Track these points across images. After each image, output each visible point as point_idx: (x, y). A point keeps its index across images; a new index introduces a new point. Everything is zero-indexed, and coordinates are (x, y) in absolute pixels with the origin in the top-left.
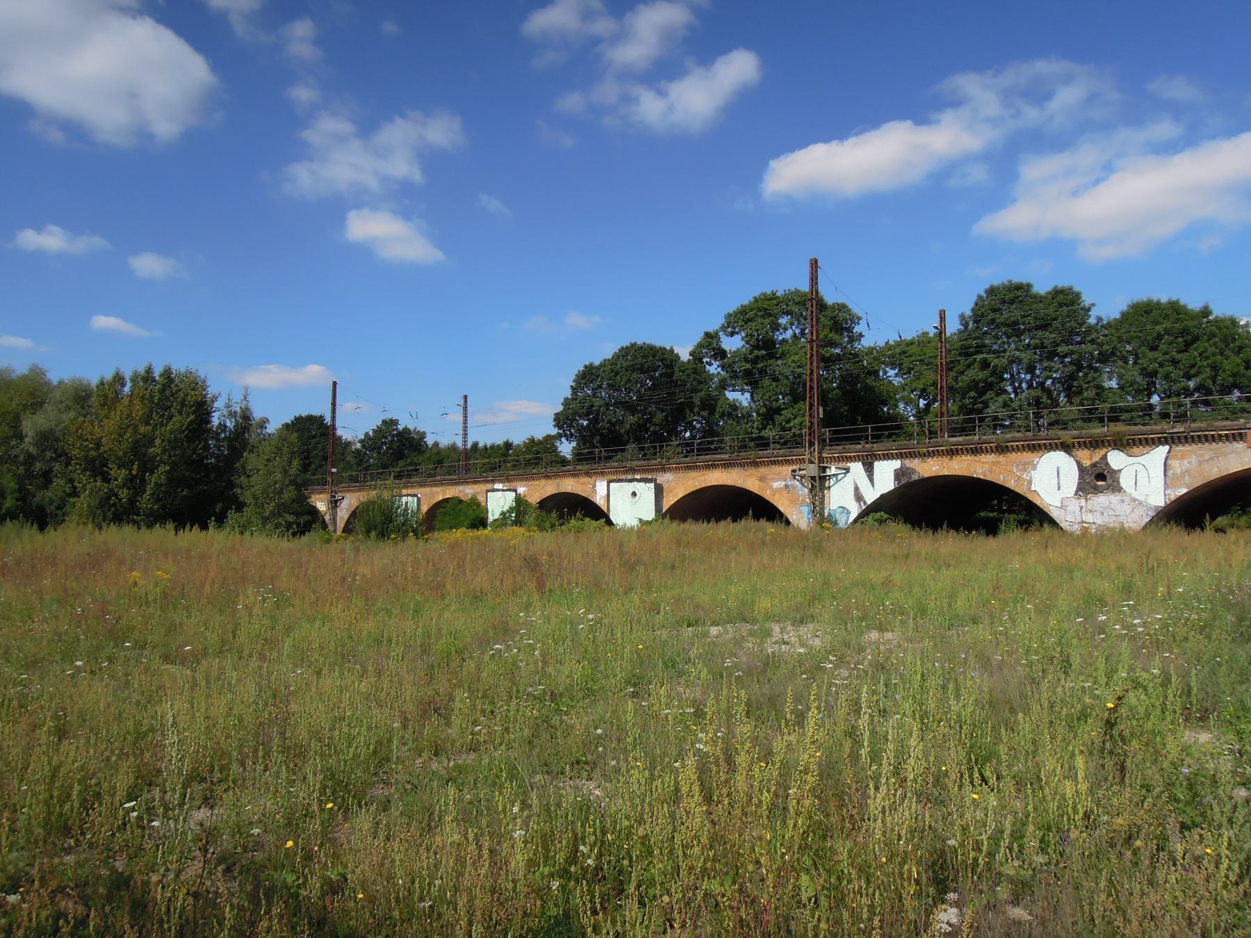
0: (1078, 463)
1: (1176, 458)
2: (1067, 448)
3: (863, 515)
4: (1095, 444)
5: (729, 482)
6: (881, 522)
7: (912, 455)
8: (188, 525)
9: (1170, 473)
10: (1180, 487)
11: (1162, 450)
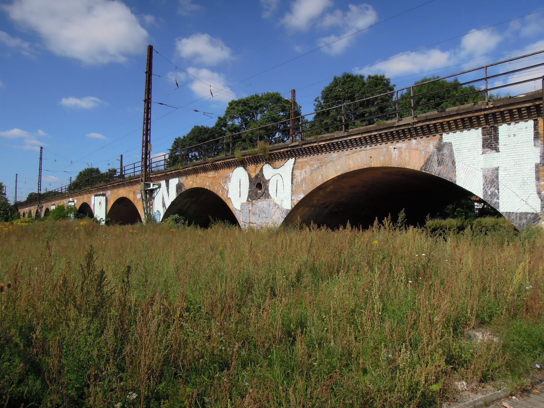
0: (249, 175)
1: (298, 169)
2: (243, 163)
3: (166, 216)
4: (256, 160)
5: (376, 163)
6: (176, 221)
7: (186, 174)
8: (376, 222)
9: (295, 180)
10: (300, 193)
11: (291, 161)
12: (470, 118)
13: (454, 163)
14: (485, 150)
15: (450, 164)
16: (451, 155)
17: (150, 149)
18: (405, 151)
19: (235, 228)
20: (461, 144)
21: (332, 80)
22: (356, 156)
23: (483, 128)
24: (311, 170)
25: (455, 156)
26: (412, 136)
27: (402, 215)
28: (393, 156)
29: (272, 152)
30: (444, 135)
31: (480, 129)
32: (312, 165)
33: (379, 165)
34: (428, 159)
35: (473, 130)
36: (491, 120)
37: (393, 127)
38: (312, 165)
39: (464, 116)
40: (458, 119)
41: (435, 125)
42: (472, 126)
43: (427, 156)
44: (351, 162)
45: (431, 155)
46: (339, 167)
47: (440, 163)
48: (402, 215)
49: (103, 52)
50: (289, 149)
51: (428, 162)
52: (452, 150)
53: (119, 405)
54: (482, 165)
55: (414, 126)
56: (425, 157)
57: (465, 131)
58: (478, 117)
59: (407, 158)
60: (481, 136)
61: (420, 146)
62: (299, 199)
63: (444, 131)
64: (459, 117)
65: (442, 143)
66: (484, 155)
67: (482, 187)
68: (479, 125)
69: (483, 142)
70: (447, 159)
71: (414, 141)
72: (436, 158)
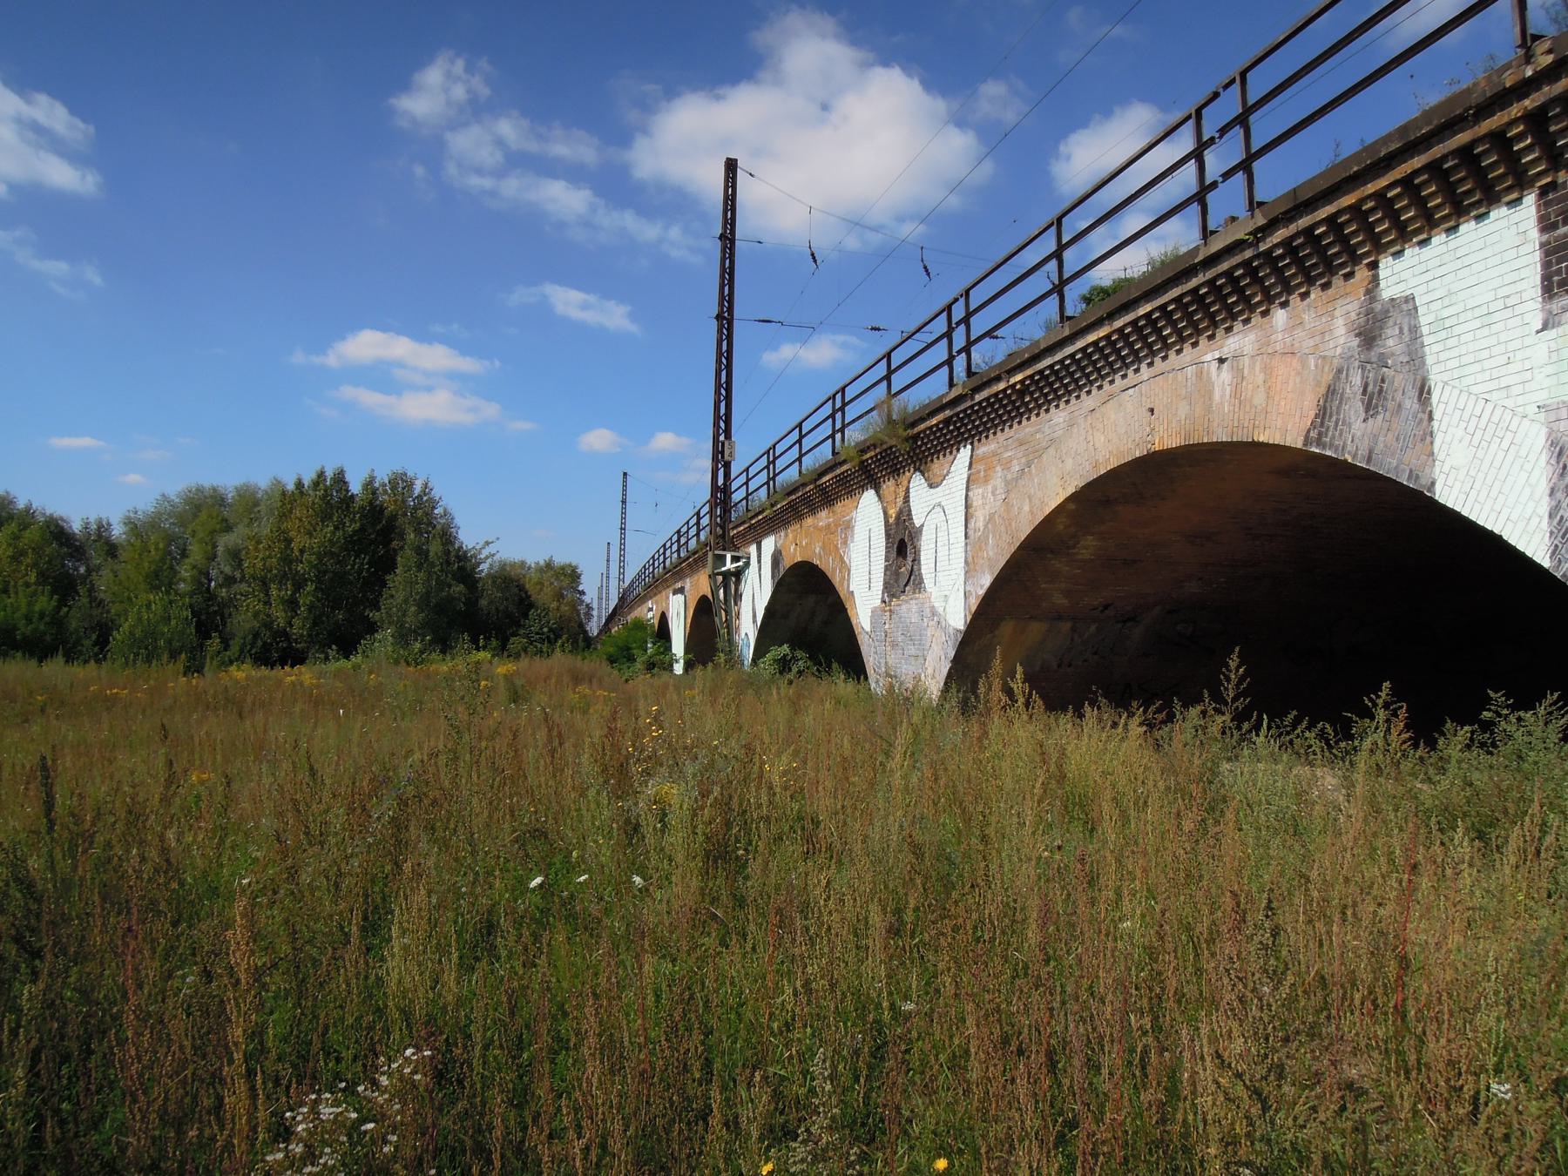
0: (885, 513)
9: (971, 525)
12: (1466, 154)
14: (1556, 305)
15: (1410, 403)
16: (1415, 358)
17: (731, 454)
18: (1252, 367)
19: (842, 686)
20: (1450, 294)
22: (1111, 413)
23: (1544, 192)
24: (1007, 483)
25: (1429, 360)
29: (916, 430)
31: (1530, 200)
32: (1007, 466)
33: (1174, 442)
35: (1499, 213)
37: (1191, 271)
38: (1007, 466)
39: (1437, 151)
40: (1416, 173)
43: (1328, 378)
44: (1100, 439)
45: (1340, 371)
46: (1069, 463)
47: (1373, 401)
49: (855, 223)
50: (948, 413)
52: (1415, 330)
53: (433, 1172)
54: (1543, 389)
55: (1263, 247)
56: (1318, 384)
57: (1468, 228)
60: (1534, 235)
61: (1299, 333)
62: (982, 592)
64: (1417, 162)
65: (1378, 307)
66: (1551, 334)
67: (1544, 507)
68: (1521, 182)
69: (1546, 265)
70: (1399, 380)
71: (1280, 316)
72: (1357, 380)
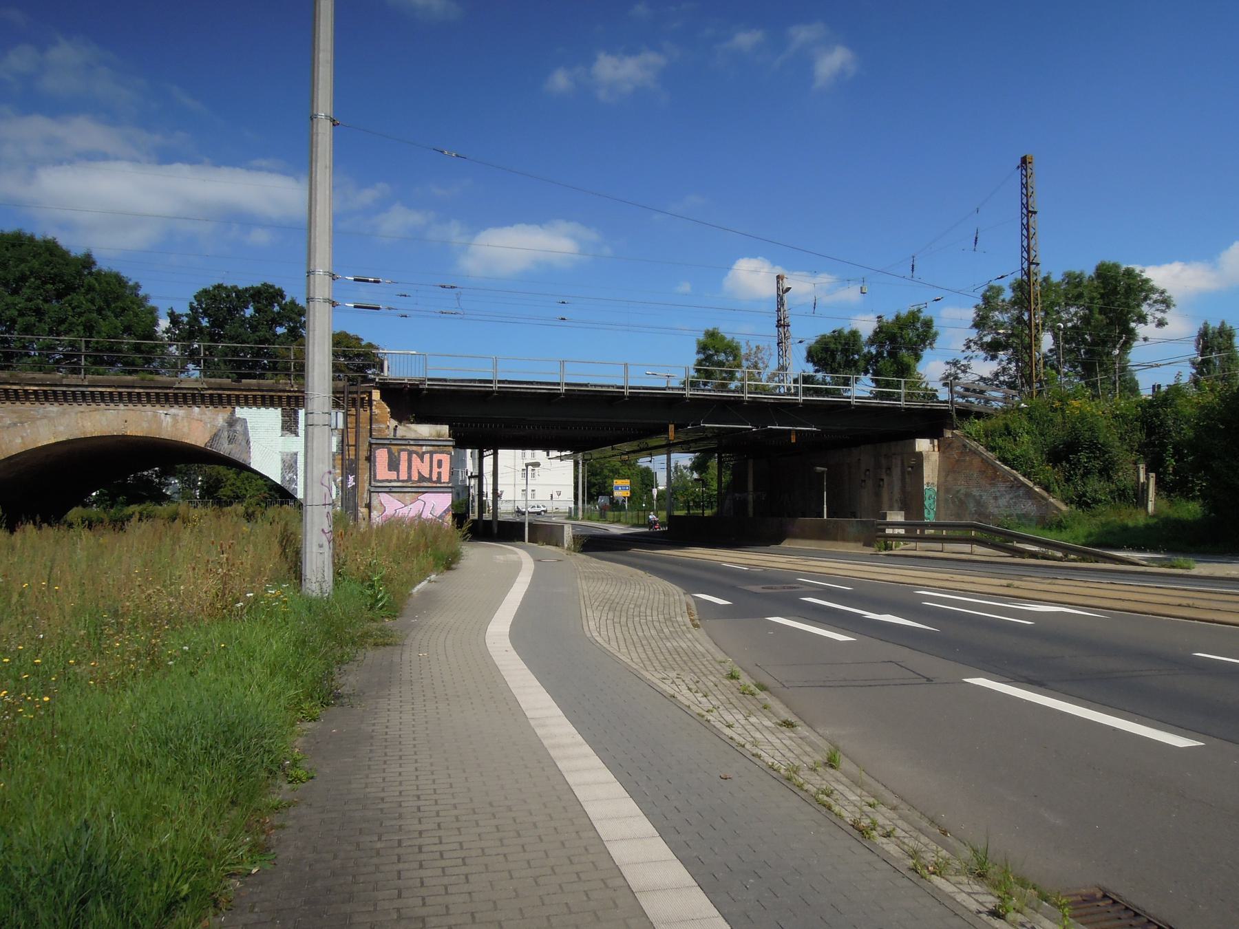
12: (272, 397)
13: (248, 442)
15: (244, 443)
16: (246, 432)
21: (1078, 272)
26: (194, 403)
27: (38, 518)
28: (164, 424)
30: (238, 409)
34: (216, 435)
35: (271, 409)
36: (293, 401)
41: (229, 396)
42: (272, 405)
43: (214, 431)
48: (38, 518)
51: (215, 437)
52: (246, 428)
57: (263, 409)
58: (280, 397)
59: (186, 430)
63: (238, 404)
